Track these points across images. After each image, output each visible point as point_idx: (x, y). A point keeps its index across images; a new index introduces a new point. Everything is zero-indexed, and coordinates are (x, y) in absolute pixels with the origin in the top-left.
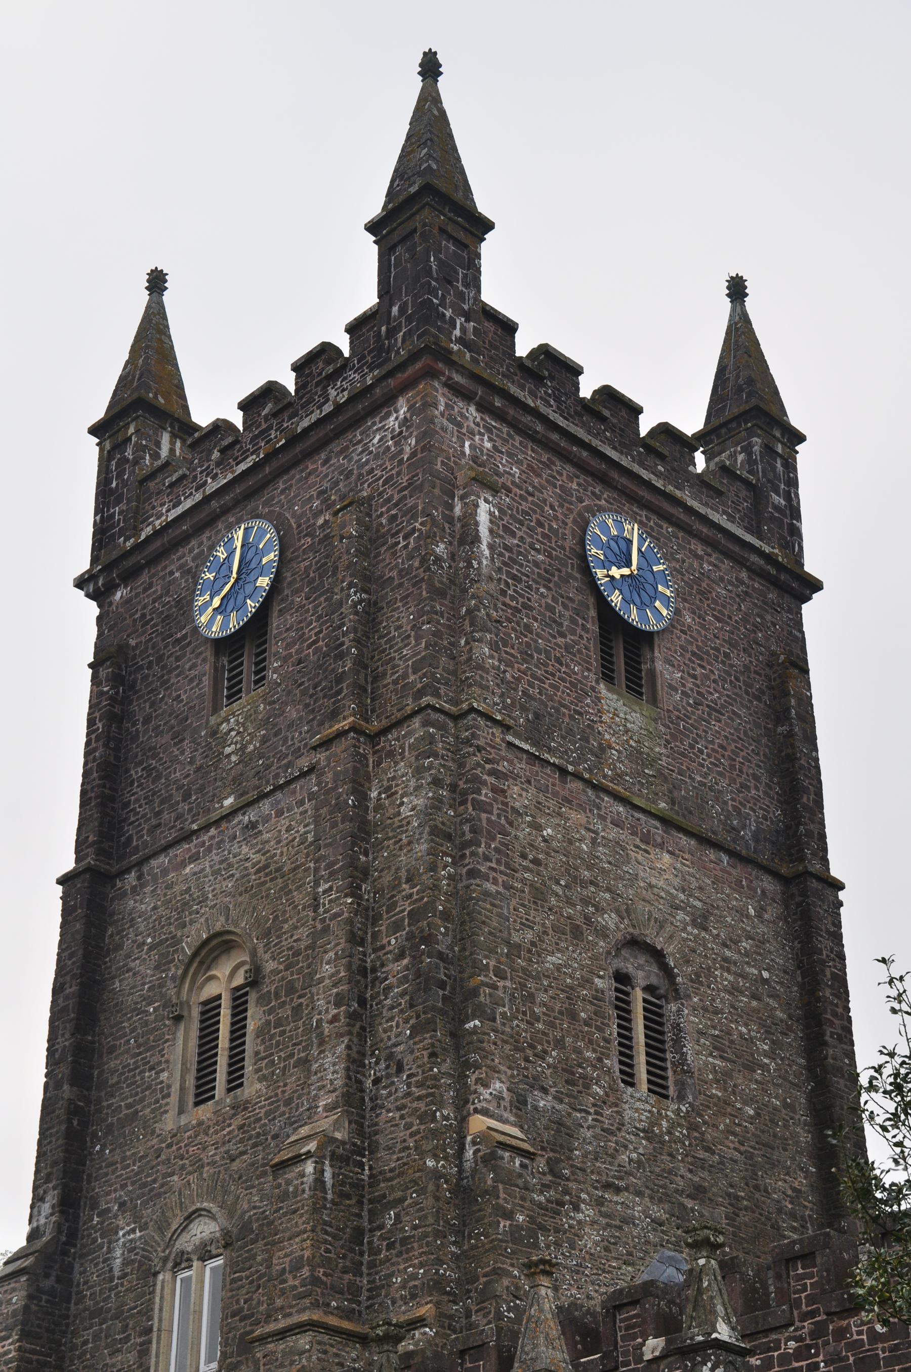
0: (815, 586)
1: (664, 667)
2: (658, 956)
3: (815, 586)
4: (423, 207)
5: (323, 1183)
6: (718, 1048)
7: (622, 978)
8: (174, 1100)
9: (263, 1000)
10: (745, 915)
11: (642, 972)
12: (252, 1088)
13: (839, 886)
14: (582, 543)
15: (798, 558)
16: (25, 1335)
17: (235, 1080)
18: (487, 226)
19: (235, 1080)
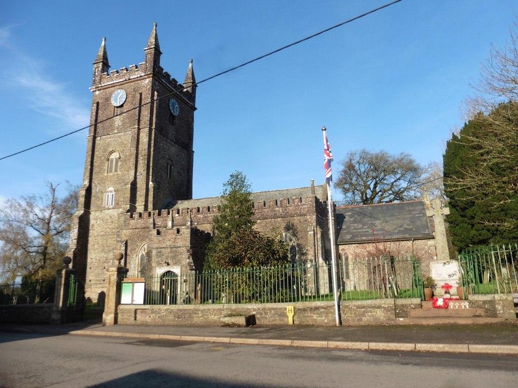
0: (196, 109)
1: (177, 121)
2: (172, 161)
3: (196, 109)
4: (331, 289)
5: (253, 333)
6: (178, 173)
7: (167, 164)
8: (106, 171)
9: (121, 161)
10: (182, 155)
11: (170, 162)
12: (119, 172)
13: (194, 152)
14: (169, 103)
15: (194, 105)
16: (85, 198)
17: (116, 170)
18: (161, 53)
19: (116, 170)
